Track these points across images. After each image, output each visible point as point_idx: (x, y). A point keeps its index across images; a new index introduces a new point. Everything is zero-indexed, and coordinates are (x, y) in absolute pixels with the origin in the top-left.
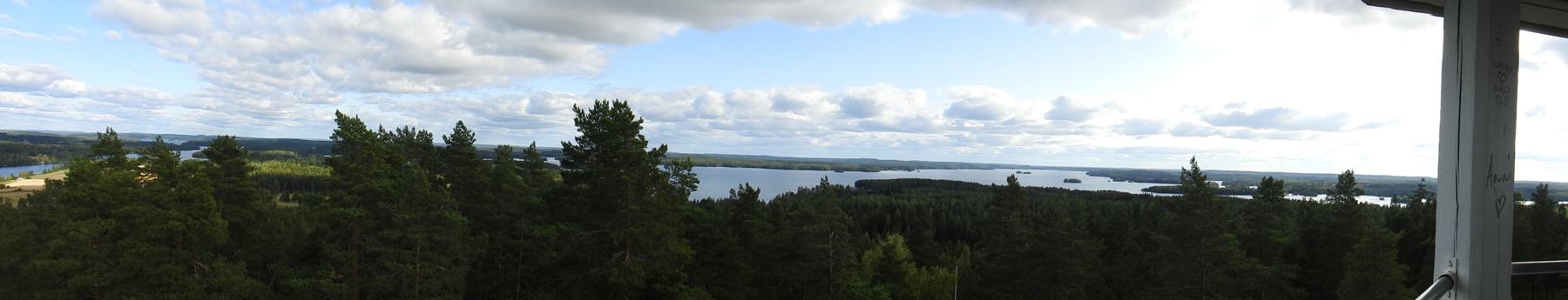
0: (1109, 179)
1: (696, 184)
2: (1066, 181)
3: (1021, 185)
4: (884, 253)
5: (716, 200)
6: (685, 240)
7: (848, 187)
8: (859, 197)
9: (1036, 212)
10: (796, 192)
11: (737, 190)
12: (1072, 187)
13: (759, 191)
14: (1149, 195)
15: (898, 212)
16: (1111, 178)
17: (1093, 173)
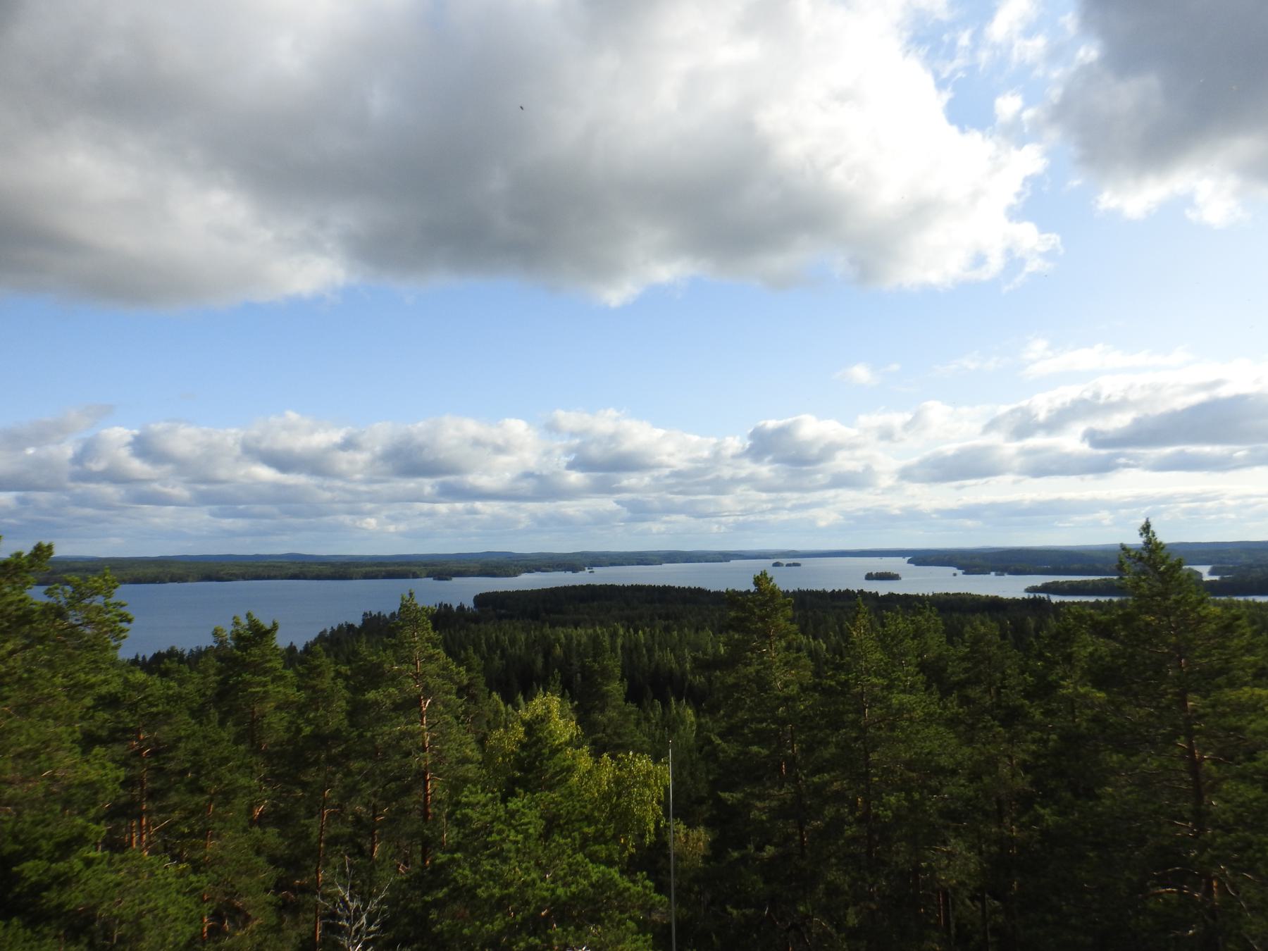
0: (954, 570)
1: (124, 625)
2: (869, 577)
4: (526, 733)
5: (187, 652)
7: (461, 608)
12: (883, 588)
13: (275, 627)
14: (1042, 601)
15: (558, 651)
16: (959, 568)
17: (922, 558)
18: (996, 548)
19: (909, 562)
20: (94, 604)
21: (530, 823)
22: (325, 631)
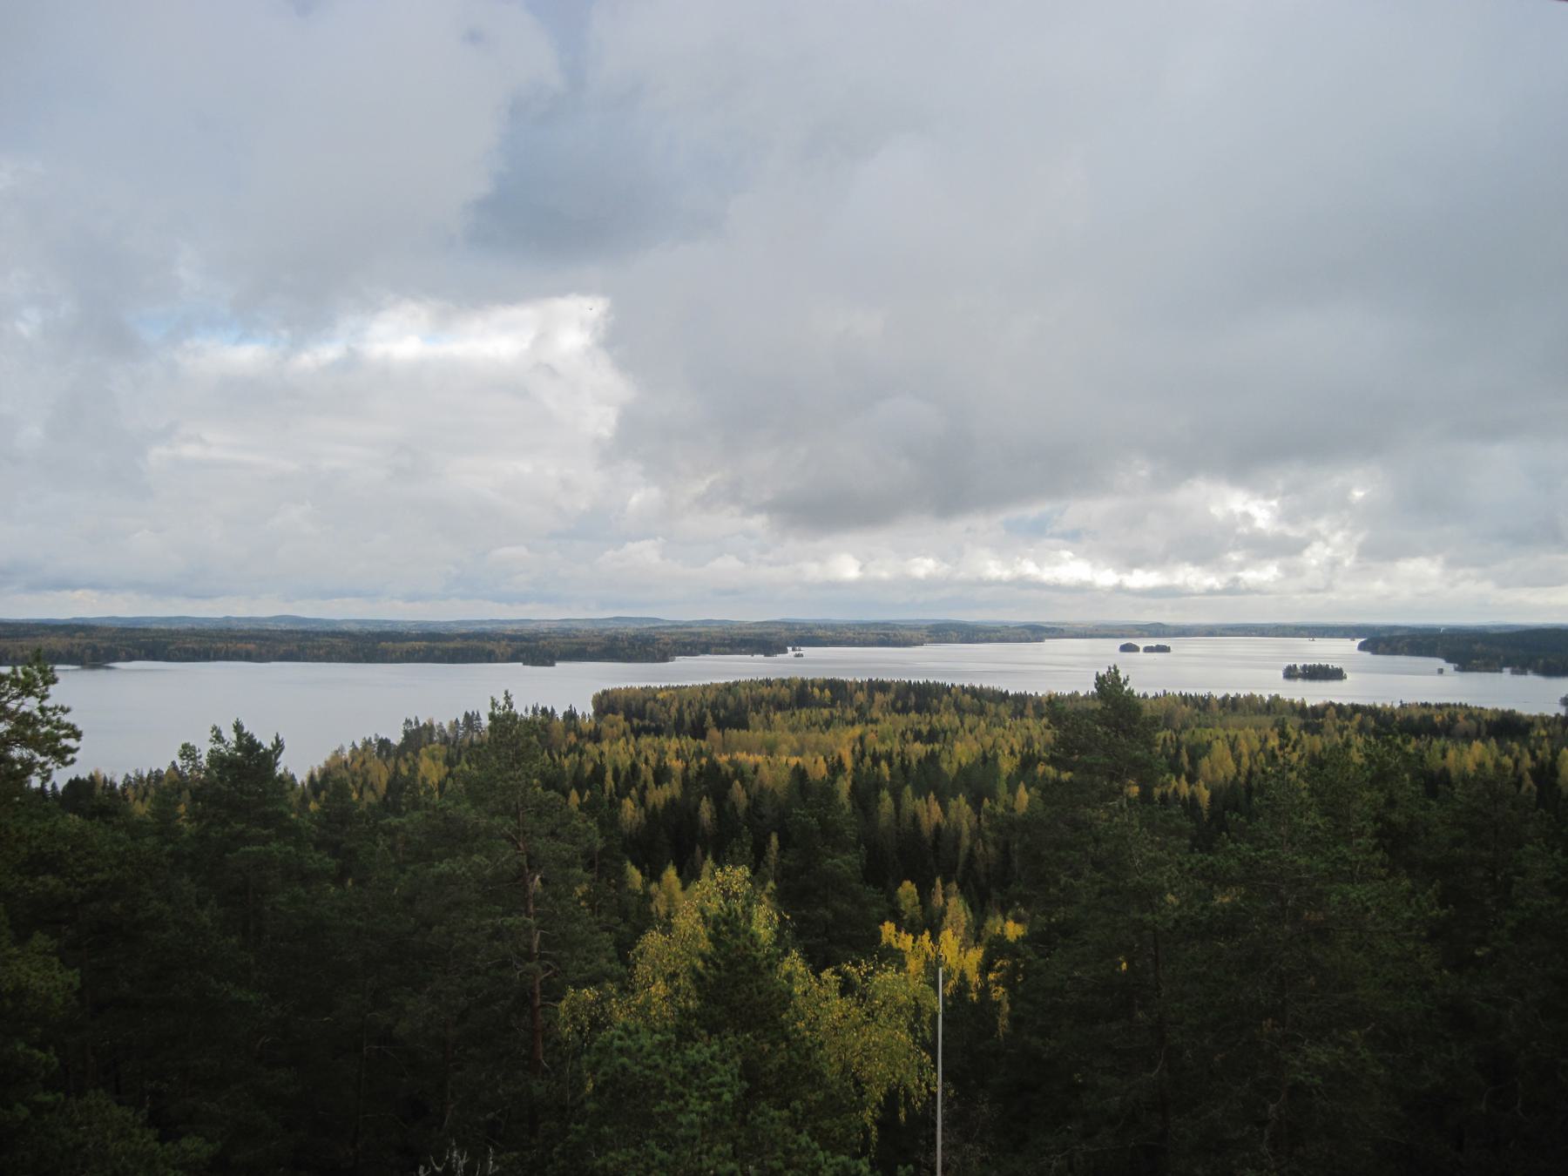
1: (71, 742)
2: (1290, 673)
3: (1138, 691)
6: (40, 940)
7: (571, 716)
8: (605, 746)
9: (1191, 779)
10: (396, 739)
11: (204, 748)
12: (1314, 694)
13: (279, 746)
15: (738, 792)
16: (1449, 660)
18: (1521, 626)
19: (1362, 647)
20: (24, 709)
21: (722, 1084)
22: (342, 749)
